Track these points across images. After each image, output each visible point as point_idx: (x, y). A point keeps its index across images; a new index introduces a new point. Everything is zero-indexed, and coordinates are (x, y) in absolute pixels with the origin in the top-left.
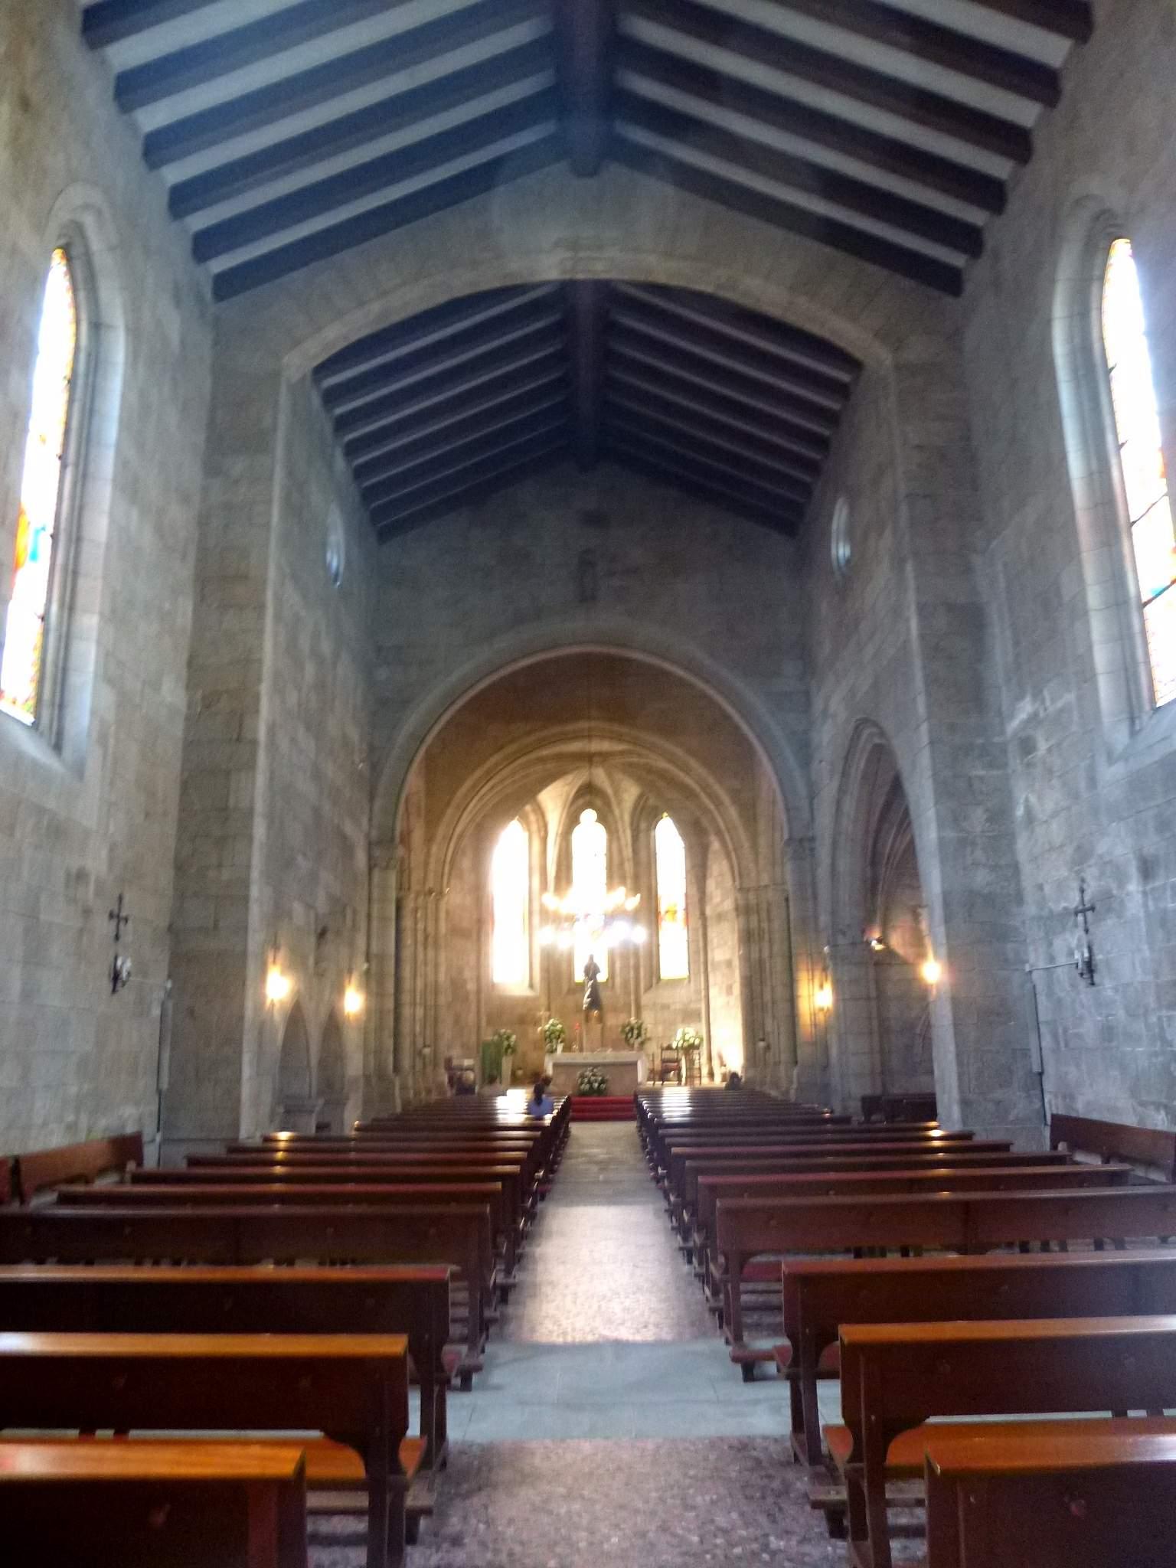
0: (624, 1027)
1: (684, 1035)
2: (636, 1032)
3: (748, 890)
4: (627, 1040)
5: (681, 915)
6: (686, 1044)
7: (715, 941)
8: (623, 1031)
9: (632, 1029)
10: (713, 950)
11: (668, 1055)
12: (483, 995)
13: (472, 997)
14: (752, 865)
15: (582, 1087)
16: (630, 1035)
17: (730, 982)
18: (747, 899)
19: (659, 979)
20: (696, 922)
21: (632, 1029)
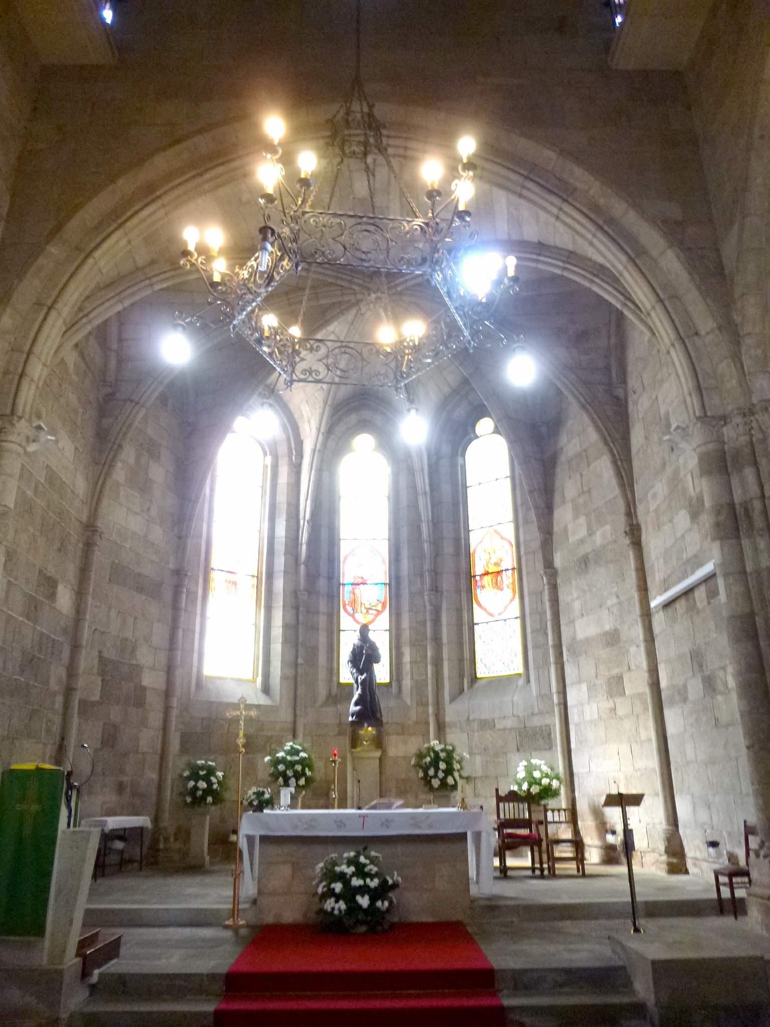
0: (420, 756)
1: (529, 769)
2: (442, 766)
3: (724, 419)
4: (427, 780)
5: (508, 579)
6: (535, 790)
7: (577, 605)
8: (418, 765)
9: (436, 760)
10: (572, 622)
11: (510, 810)
12: (175, 702)
13: (154, 702)
14: (726, 368)
15: (330, 904)
16: (431, 772)
17: (615, 671)
18: (720, 441)
19: (474, 679)
20: (538, 581)
21: (436, 760)
